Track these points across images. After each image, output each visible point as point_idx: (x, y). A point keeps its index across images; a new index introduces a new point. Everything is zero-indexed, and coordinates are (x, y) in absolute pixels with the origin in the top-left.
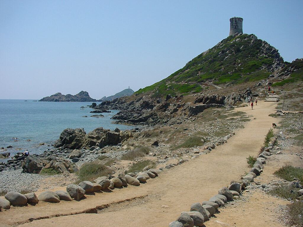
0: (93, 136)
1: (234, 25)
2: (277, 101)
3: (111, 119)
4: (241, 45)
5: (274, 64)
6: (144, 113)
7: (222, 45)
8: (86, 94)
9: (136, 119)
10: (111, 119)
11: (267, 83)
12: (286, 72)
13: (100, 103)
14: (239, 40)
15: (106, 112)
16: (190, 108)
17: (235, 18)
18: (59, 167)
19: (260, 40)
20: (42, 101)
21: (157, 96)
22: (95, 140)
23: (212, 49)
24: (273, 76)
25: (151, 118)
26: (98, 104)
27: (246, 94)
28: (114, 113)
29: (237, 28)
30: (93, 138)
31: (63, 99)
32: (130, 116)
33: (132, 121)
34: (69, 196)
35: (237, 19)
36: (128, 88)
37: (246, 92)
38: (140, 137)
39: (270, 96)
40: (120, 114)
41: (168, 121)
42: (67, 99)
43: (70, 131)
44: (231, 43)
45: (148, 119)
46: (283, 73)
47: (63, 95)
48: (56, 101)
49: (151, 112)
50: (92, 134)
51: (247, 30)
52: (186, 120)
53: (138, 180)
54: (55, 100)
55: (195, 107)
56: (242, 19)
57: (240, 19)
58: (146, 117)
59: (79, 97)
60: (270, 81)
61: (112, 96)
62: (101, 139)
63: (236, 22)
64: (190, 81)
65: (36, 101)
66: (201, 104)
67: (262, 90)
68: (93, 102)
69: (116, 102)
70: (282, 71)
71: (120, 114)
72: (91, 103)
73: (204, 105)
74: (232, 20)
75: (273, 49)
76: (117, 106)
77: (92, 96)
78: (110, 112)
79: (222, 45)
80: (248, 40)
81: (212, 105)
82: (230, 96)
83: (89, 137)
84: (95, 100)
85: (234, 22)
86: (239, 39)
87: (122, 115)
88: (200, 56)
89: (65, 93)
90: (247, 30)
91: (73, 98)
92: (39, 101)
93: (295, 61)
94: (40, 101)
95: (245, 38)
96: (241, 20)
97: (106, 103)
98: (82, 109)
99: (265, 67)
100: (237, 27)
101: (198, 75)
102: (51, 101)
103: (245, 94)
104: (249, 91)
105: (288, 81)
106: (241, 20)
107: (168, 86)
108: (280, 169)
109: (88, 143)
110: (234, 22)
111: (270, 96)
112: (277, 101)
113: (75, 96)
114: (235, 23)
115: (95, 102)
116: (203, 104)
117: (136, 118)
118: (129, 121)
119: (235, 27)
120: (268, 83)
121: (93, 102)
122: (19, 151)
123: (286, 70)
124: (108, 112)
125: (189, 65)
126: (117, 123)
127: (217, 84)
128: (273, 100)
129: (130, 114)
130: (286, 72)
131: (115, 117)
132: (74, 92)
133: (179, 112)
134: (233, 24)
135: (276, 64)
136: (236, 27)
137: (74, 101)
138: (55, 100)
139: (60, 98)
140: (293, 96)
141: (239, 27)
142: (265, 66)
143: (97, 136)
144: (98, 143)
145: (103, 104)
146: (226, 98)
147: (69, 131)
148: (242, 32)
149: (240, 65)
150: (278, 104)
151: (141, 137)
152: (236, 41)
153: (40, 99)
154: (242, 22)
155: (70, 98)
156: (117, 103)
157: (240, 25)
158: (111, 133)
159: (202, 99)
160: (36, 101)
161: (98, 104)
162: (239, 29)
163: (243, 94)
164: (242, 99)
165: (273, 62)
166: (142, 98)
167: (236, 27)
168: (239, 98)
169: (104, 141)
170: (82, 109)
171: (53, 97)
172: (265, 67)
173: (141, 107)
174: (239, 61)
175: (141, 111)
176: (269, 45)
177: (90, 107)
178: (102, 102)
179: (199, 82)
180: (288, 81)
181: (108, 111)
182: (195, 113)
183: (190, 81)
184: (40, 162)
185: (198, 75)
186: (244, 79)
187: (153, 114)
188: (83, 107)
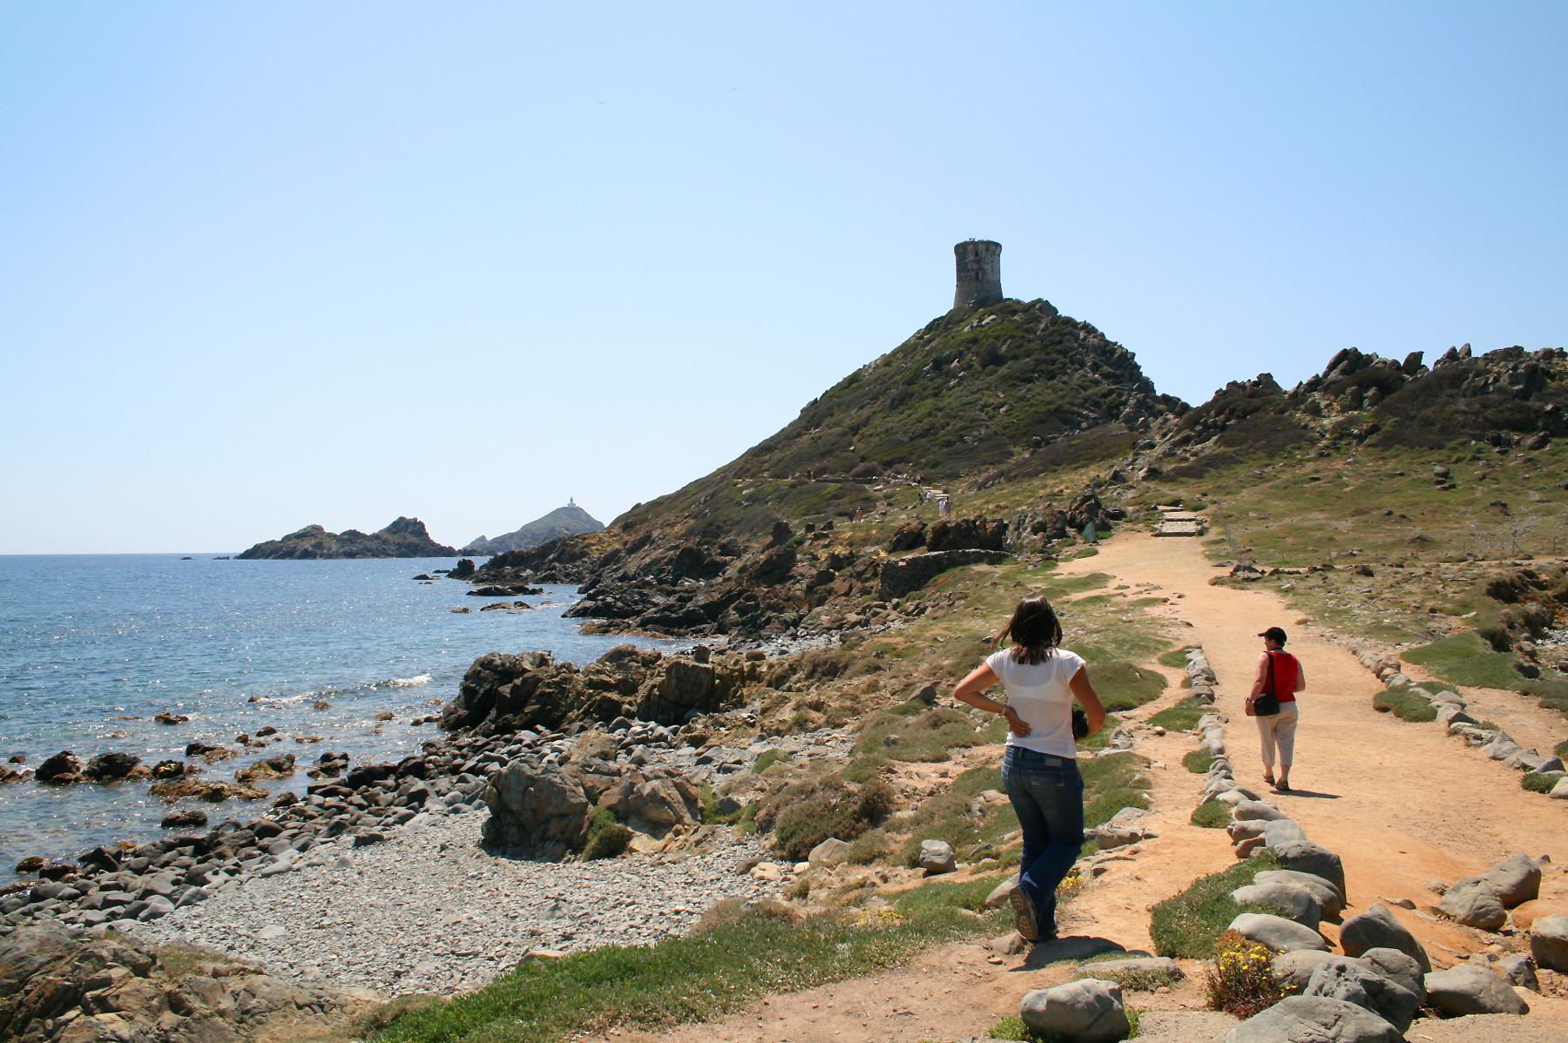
1: (969, 266)
2: (1201, 533)
3: (564, 616)
7: (930, 341)
8: (417, 528)
10: (564, 616)
12: (1199, 428)
13: (486, 559)
17: (973, 243)
19: (1069, 321)
23: (894, 353)
24: (1151, 446)
26: (479, 562)
27: (1081, 509)
30: (606, 686)
31: (330, 549)
32: (636, 603)
35: (982, 248)
37: (1080, 505)
38: (794, 678)
39: (1168, 515)
40: (601, 597)
41: (801, 617)
43: (503, 664)
44: (966, 329)
46: (1186, 432)
47: (330, 535)
48: (306, 555)
49: (728, 588)
54: (301, 553)
55: (904, 564)
56: (998, 245)
59: (391, 538)
61: (511, 535)
63: (977, 255)
65: (228, 558)
66: (921, 553)
69: (551, 557)
71: (601, 597)
74: (962, 250)
75: (1119, 351)
76: (554, 568)
79: (930, 341)
82: (1024, 521)
83: (591, 684)
85: (971, 257)
86: (992, 317)
87: (609, 599)
88: (854, 379)
89: (335, 526)
90: (1016, 285)
91: (368, 544)
95: (1014, 313)
96: (993, 248)
99: (1095, 415)
101: (852, 448)
102: (282, 557)
103: (1081, 513)
104: (1093, 501)
105: (1214, 462)
106: (993, 248)
107: (744, 492)
108: (1144, 784)
109: (590, 706)
112: (1201, 533)
113: (376, 537)
115: (467, 558)
120: (1145, 469)
125: (814, 414)
126: (604, 630)
127: (925, 481)
130: (1199, 428)
131: (579, 607)
132: (372, 523)
133: (839, 584)
134: (966, 264)
136: (977, 274)
137: (375, 554)
138: (298, 553)
139: (319, 546)
141: (990, 276)
142: (1093, 412)
143: (618, 677)
145: (498, 563)
146: (1011, 527)
147: (498, 662)
149: (1007, 411)
150: (1203, 544)
151: (800, 675)
152: (983, 323)
155: (353, 545)
156: (555, 559)
160: (228, 558)
161: (479, 562)
164: (1071, 531)
165: (1123, 398)
167: (977, 274)
168: (1058, 526)
169: (660, 696)
171: (292, 544)
172: (1095, 415)
176: (1102, 335)
177: (452, 575)
180: (1214, 462)
183: (823, 470)
185: (852, 448)
186: (1431, 437)
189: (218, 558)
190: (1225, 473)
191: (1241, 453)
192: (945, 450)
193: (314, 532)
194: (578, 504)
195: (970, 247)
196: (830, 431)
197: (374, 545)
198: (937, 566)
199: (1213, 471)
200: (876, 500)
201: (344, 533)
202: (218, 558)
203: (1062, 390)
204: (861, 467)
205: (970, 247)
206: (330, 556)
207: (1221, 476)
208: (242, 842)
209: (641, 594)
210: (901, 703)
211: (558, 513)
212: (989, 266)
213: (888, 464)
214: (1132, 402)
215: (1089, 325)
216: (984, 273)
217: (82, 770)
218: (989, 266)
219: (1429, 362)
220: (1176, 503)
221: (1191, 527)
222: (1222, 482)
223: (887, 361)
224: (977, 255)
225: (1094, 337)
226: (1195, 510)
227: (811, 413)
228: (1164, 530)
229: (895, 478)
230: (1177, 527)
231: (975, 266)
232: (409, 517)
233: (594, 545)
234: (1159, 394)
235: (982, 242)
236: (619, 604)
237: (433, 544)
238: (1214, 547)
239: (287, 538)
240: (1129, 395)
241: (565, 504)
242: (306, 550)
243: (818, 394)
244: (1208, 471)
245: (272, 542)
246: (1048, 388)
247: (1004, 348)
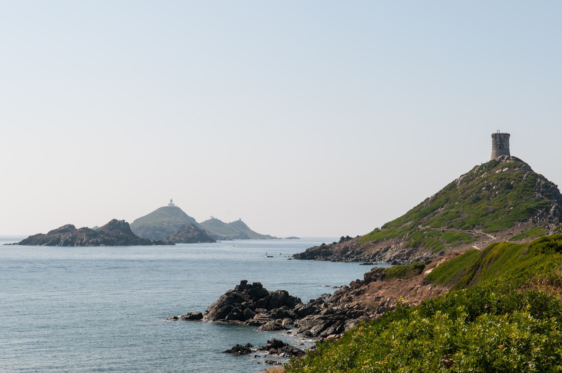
17: (499, 134)
20: (24, 244)
29: (502, 148)
35: (502, 136)
36: (169, 203)
42: (94, 240)
51: (515, 151)
56: (509, 135)
57: (506, 136)
63: (500, 139)
74: (495, 136)
96: (507, 136)
106: (507, 136)
110: (499, 140)
114: (500, 141)
119: (499, 146)
141: (505, 147)
148: (509, 154)
166: (390, 247)
167: (500, 146)
193: (70, 228)
194: (177, 204)
195: (498, 136)
205: (498, 136)
206: (82, 244)
210: (538, 238)
211: (163, 210)
214: (553, 207)
216: (503, 146)
218: (505, 143)
232: (119, 219)
235: (502, 134)
240: (553, 204)
241: (166, 204)
243: (441, 189)
245: (40, 235)
247: (512, 182)
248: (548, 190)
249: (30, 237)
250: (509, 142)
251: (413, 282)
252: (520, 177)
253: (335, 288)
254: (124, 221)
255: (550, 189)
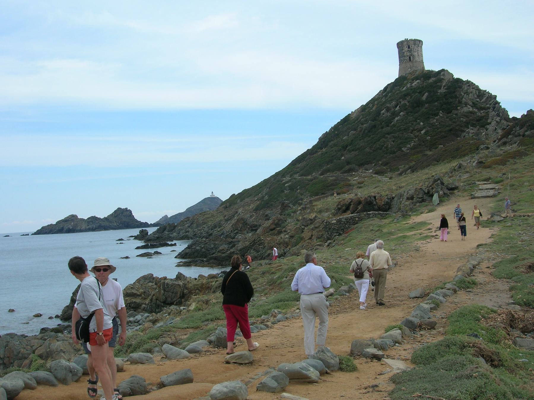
0: (134, 291)
1: (405, 54)
4: (421, 93)
5: (490, 123)
6: (239, 241)
9: (224, 255)
11: (474, 162)
13: (155, 229)
14: (418, 83)
15: (167, 245)
16: (326, 223)
17: (406, 40)
18: (61, 350)
19: (459, 80)
21: (266, 205)
22: (138, 300)
23: (368, 104)
25: (254, 250)
28: (181, 246)
33: (215, 258)
34: (52, 378)
39: (481, 187)
45: (247, 253)
48: (69, 231)
49: (253, 239)
50: (132, 288)
52: (318, 247)
53: (186, 352)
55: (335, 221)
56: (420, 42)
57: (417, 43)
58: (244, 248)
60: (481, 158)
61: (180, 214)
62: (150, 297)
63: (409, 48)
64: (328, 171)
65: (28, 235)
66: (348, 215)
67: (466, 176)
68: (141, 229)
70: (503, 137)
72: (136, 232)
73: (353, 215)
74: (400, 45)
77: (139, 216)
78: (175, 244)
80: (436, 82)
81: (368, 214)
84: (146, 225)
85: (406, 49)
86: (417, 81)
87: (198, 248)
89: (84, 215)
92: (32, 234)
93: (526, 114)
94: (35, 234)
96: (418, 43)
97: (168, 228)
98: (120, 243)
100: (411, 57)
105: (518, 155)
106: (418, 43)
110: (407, 49)
111: (481, 188)
113: (106, 219)
114: (408, 51)
115: (144, 229)
116: (352, 213)
117: (223, 253)
118: (211, 259)
119: (408, 57)
120: (476, 162)
121: (141, 229)
122: (323, 336)
123: (510, 134)
124: (172, 245)
128: (488, 195)
129: (212, 246)
132: (103, 213)
133: (306, 234)
135: (494, 123)
136: (410, 57)
137: (106, 228)
140: (525, 184)
141: (417, 59)
144: (145, 304)
149: (425, 132)
153: (39, 228)
154: (421, 47)
157: (418, 54)
158: (167, 284)
159: (350, 204)
160: (28, 235)
162: (416, 62)
163: (428, 187)
166: (237, 212)
167: (410, 57)
170: (120, 243)
173: (234, 231)
174: (422, 123)
175: (234, 238)
177: (136, 238)
178: (159, 227)
179: (345, 172)
181: (170, 243)
182: (337, 233)
184: (27, 345)
187: (257, 242)
188: (122, 240)
189: (23, 235)
190: (518, 161)
191: (528, 149)
192: (392, 155)
193: (73, 218)
196: (332, 149)
197: (106, 224)
198: (353, 222)
199: (511, 161)
200: (353, 186)
201: (89, 218)
202: (23, 235)
203: (455, 119)
204: (347, 167)
207: (515, 163)
208: (315, 384)
209: (215, 244)
212: (416, 53)
213: (361, 165)
215: (470, 81)
216: (414, 57)
217: (143, 348)
218: (416, 53)
219: (487, 91)
220: (487, 180)
221: (491, 193)
222: (515, 167)
223: (363, 108)
224: (409, 48)
225: (473, 88)
226: (497, 183)
227: (323, 140)
228: (476, 195)
229: (365, 173)
230: (484, 194)
231: (408, 54)
232: (123, 207)
233: (209, 218)
234: (511, 117)
235: (411, 40)
236: (203, 250)
237: (137, 221)
238: (498, 203)
239: (59, 222)
242: (69, 228)
244: (509, 161)
246: (447, 118)
248: (482, 101)
249: (43, 228)
250: (421, 51)
251: (154, 304)
252: (503, 144)
253: (487, 268)
254: (127, 208)
255: (484, 99)
